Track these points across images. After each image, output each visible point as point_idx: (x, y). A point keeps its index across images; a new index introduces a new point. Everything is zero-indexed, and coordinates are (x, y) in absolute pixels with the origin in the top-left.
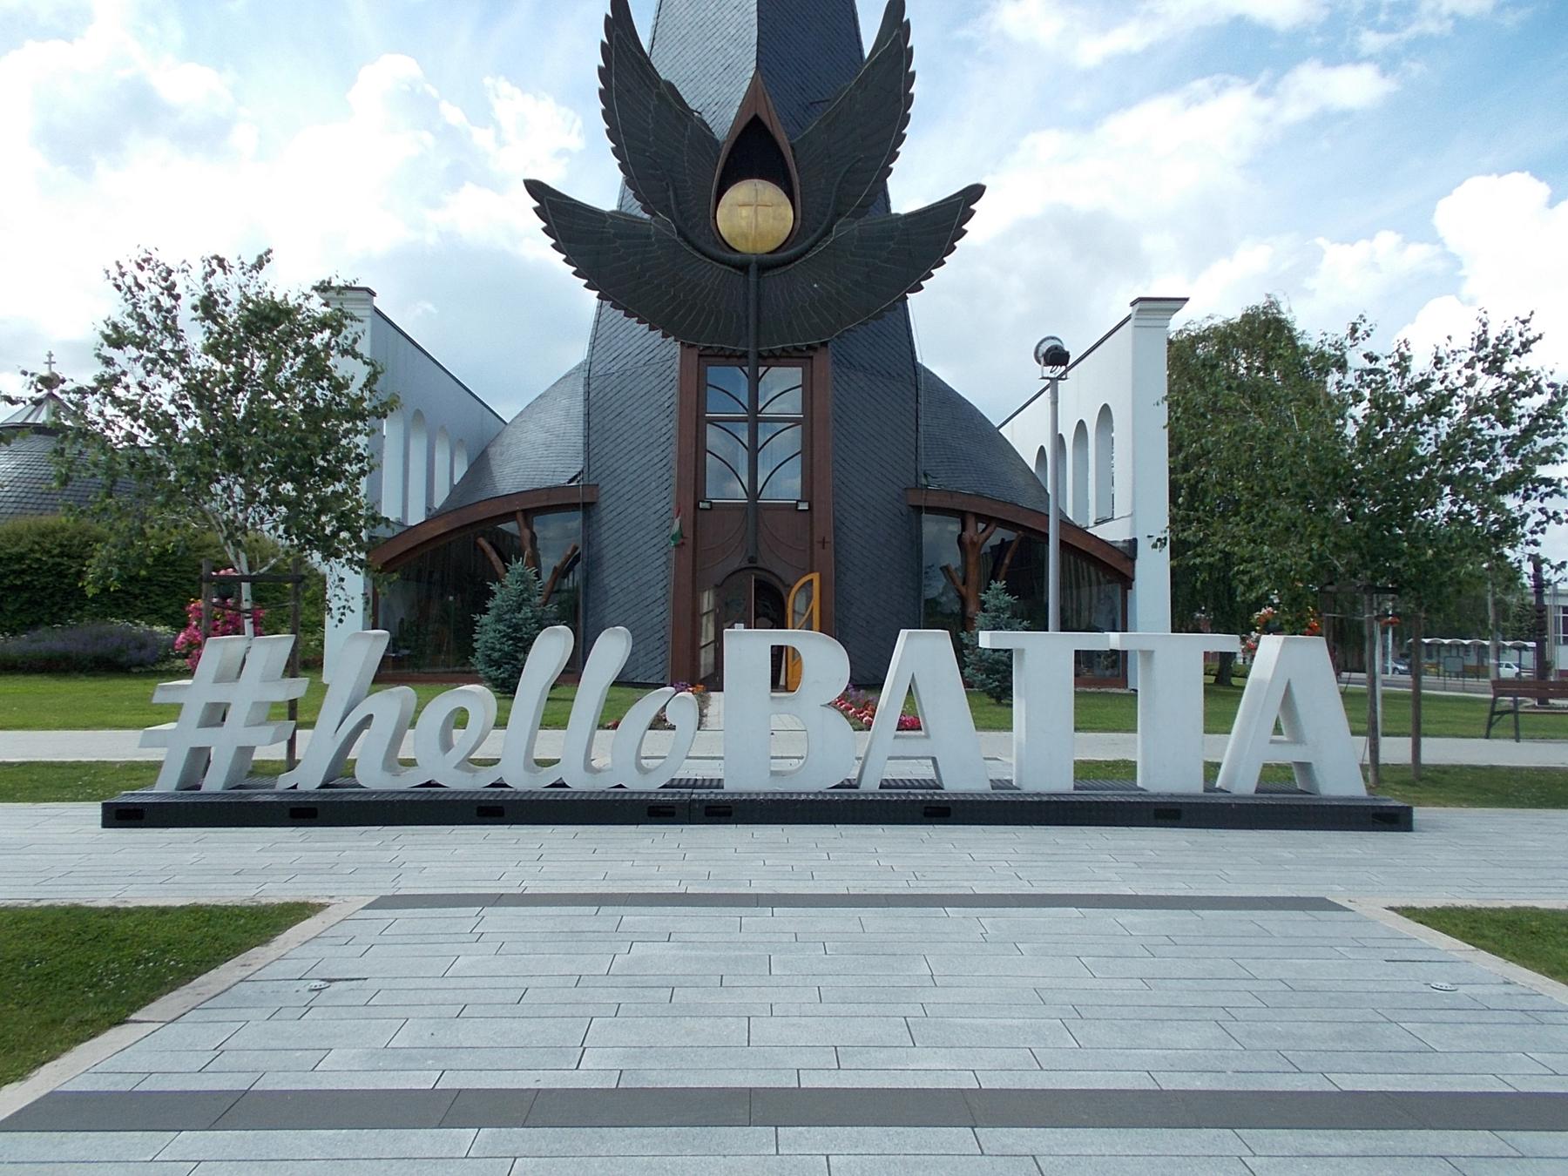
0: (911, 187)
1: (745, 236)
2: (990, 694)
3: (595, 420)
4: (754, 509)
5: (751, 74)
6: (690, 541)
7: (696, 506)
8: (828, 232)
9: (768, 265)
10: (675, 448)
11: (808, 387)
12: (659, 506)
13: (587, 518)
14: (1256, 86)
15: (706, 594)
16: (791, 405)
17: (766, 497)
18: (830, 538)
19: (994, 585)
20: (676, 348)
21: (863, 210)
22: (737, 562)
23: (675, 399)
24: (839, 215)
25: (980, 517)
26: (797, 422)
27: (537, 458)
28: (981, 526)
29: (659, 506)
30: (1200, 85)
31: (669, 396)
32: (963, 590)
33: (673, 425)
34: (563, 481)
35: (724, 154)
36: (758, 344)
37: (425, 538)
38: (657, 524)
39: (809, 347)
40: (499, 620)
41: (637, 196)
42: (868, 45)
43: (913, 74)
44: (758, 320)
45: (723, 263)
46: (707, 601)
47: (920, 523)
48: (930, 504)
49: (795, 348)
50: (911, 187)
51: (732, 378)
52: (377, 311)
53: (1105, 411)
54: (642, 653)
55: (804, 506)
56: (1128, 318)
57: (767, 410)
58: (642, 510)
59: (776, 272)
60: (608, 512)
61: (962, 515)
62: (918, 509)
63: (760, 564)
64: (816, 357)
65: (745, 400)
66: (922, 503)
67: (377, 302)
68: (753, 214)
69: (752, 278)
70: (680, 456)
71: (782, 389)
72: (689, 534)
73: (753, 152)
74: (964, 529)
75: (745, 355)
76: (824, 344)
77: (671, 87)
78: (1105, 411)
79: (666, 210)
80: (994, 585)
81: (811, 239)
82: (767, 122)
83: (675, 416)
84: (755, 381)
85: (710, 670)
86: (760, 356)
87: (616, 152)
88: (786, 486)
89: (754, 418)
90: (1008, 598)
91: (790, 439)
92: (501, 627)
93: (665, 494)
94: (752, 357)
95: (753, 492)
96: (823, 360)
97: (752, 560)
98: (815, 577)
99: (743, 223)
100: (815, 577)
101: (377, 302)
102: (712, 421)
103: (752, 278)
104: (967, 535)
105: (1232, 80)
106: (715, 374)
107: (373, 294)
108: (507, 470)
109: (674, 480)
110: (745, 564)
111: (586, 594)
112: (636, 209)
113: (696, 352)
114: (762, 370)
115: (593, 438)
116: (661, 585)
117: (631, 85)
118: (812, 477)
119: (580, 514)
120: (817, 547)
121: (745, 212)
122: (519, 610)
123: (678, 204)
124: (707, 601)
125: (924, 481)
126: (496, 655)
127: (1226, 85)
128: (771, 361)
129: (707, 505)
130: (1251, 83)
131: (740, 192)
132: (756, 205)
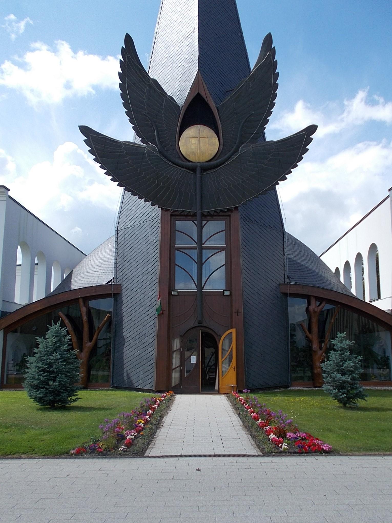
0: (282, 124)
1: (194, 153)
2: (340, 401)
3: (120, 252)
4: (201, 295)
5: (196, 73)
6: (166, 313)
7: (170, 293)
8: (237, 151)
9: (207, 168)
10: (158, 263)
11: (228, 231)
12: (151, 294)
13: (116, 301)
14: (381, 145)
15: (176, 340)
16: (219, 241)
17: (207, 288)
18: (241, 310)
19: (339, 335)
20: (159, 211)
21: (255, 139)
22: (192, 323)
23: (159, 238)
24: (242, 143)
25: (317, 298)
26: (222, 249)
27: (95, 271)
28: (318, 303)
29: (151, 294)
30: (360, 145)
31: (156, 237)
32: (310, 336)
33: (158, 251)
34: (104, 283)
35: (182, 112)
36: (202, 208)
37: (30, 313)
38: (150, 303)
39: (229, 210)
40: (40, 359)
41: (138, 135)
42: (253, 61)
43: (278, 73)
44: (202, 197)
45: (183, 167)
46: (176, 344)
47: (287, 301)
48: (291, 292)
49: (221, 211)
50: (282, 124)
51: (187, 226)
52: (10, 197)
53: (373, 247)
54: (141, 373)
55: (227, 293)
56: (388, 197)
57: (208, 243)
58: (142, 296)
59: (211, 171)
60: (126, 298)
61: (308, 297)
62: (286, 295)
63: (204, 324)
64: (232, 215)
65: (195, 238)
66: (288, 292)
67: (10, 193)
68: (198, 143)
69: (198, 175)
70: (161, 267)
71: (214, 231)
72: (166, 308)
73: (197, 110)
74: (309, 304)
75: (195, 215)
76: (236, 208)
77: (155, 81)
78: (373, 247)
79: (153, 142)
80: (339, 335)
81: (229, 154)
82: (205, 97)
83: (159, 246)
84: (200, 228)
85: (178, 382)
86: (203, 215)
87: (128, 114)
88: (216, 282)
89: (201, 247)
90: (348, 342)
91: (219, 259)
92: (40, 365)
93: (154, 287)
94: (198, 215)
95: (200, 286)
96: (236, 217)
97: (200, 322)
98: (233, 331)
99: (193, 147)
100: (233, 331)
101: (10, 193)
102: (178, 249)
103: (198, 175)
104: (311, 308)
105: (371, 143)
106: (179, 224)
107: (9, 190)
108: (78, 278)
109: (158, 280)
110: (196, 324)
111: (115, 341)
112: (138, 141)
113: (169, 213)
114: (204, 222)
115: (119, 260)
116: (152, 336)
117: (136, 82)
118: (231, 278)
119: (112, 299)
120: (234, 315)
121: (193, 141)
122: (51, 354)
123: (159, 139)
124: (176, 344)
125: (287, 280)
126: (36, 382)
127: (369, 145)
128: (209, 218)
129: (176, 293)
130: (378, 144)
131: (190, 132)
132: (199, 138)
